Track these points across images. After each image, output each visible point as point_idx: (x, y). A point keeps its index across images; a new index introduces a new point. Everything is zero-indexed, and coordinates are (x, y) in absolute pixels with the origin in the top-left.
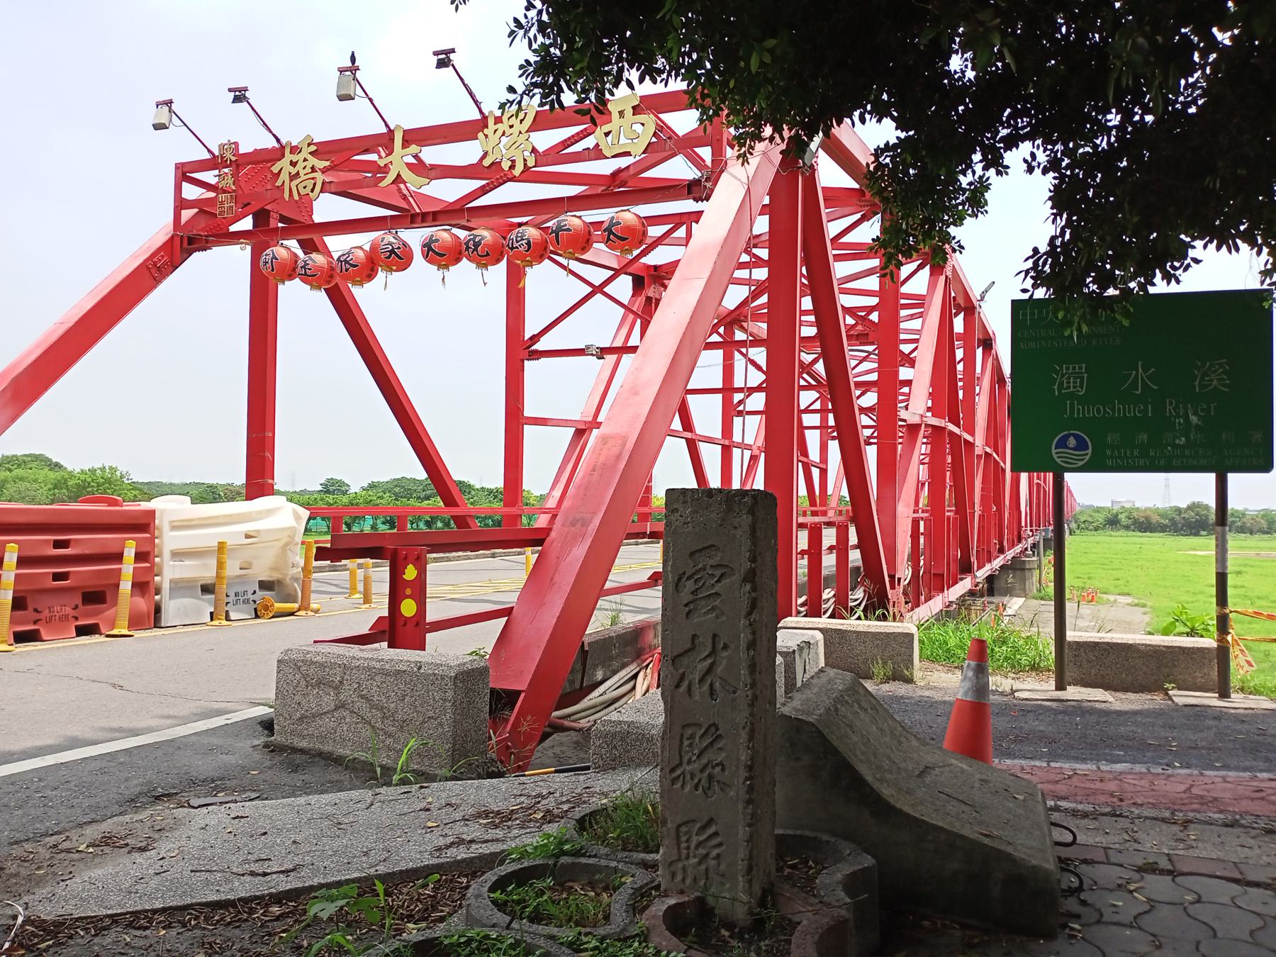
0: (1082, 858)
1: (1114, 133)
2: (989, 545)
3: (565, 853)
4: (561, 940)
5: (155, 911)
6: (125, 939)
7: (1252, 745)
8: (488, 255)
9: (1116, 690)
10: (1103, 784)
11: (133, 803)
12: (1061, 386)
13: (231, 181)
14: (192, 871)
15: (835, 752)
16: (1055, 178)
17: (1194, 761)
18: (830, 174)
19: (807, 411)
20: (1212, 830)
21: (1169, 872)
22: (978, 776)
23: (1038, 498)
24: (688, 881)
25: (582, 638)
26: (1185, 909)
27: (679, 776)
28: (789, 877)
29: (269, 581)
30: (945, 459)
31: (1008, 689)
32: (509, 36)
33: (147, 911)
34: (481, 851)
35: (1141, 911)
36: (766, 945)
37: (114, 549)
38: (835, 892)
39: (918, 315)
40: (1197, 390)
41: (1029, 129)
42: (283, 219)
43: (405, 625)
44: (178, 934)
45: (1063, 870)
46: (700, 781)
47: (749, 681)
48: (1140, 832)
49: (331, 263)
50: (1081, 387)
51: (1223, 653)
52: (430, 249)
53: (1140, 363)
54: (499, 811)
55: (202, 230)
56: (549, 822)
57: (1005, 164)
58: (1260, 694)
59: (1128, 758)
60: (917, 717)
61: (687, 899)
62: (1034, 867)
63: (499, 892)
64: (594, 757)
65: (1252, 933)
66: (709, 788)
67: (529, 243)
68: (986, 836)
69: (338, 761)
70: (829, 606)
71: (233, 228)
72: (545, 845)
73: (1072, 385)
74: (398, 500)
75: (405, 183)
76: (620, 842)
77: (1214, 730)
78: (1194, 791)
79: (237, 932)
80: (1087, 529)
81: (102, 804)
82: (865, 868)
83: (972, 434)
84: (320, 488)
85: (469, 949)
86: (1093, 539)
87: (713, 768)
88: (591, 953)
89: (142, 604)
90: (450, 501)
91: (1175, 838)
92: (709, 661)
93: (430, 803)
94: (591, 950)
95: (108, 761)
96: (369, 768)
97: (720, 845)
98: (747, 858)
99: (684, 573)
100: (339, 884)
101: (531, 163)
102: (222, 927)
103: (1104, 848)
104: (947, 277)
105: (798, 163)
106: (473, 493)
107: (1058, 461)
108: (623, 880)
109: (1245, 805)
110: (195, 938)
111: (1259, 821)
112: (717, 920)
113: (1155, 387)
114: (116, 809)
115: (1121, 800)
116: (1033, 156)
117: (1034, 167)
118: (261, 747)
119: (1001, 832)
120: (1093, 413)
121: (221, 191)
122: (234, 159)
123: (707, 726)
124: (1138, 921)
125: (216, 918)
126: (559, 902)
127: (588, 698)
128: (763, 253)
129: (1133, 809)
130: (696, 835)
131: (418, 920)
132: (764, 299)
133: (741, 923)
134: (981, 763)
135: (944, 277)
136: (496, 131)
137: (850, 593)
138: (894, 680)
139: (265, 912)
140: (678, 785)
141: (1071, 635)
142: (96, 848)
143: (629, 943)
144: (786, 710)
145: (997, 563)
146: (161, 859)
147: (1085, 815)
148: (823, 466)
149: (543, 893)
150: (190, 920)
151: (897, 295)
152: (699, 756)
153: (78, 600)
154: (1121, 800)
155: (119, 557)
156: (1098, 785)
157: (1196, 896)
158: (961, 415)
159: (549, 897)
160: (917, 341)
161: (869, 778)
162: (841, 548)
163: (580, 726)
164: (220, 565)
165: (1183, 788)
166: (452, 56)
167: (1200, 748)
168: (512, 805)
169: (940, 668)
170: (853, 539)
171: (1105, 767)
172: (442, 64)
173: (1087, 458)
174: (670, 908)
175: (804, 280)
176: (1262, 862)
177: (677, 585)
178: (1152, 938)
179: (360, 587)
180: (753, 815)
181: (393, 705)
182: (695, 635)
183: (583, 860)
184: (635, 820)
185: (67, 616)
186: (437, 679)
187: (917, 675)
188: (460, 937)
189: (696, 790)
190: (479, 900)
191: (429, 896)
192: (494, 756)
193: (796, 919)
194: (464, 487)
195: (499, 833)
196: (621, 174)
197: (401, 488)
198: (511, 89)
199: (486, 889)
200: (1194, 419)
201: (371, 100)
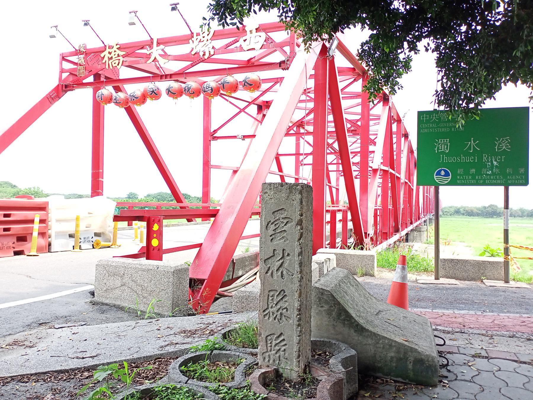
0: (448, 351)
1: (463, 34)
2: (406, 221)
3: (216, 349)
4: (210, 389)
5: (32, 375)
6: (16, 387)
7: (520, 303)
8: (194, 93)
9: (460, 280)
10: (456, 319)
11: (29, 326)
12: (438, 149)
13: (83, 61)
14: (51, 356)
15: (339, 304)
16: (438, 54)
17: (495, 309)
18: (341, 61)
19: (331, 164)
20: (504, 339)
21: (486, 357)
22: (402, 315)
23: (427, 202)
24: (271, 361)
25: (232, 257)
26: (494, 374)
27: (267, 314)
28: (317, 360)
29: (99, 233)
30: (388, 185)
31: (415, 279)
32: (207, 8)
33: (28, 374)
34: (180, 348)
35: (475, 375)
36: (306, 391)
37: (30, 218)
38: (338, 366)
39: (377, 123)
40: (497, 150)
41: (427, 33)
42: (106, 78)
43: (153, 250)
44: (41, 385)
45: (440, 356)
46: (276, 316)
47: (299, 270)
48: (473, 340)
49: (127, 97)
50: (447, 149)
51: (506, 264)
52: (169, 91)
53: (472, 139)
54: (190, 330)
55: (71, 82)
56: (212, 335)
57: (418, 49)
58: (522, 281)
59: (466, 308)
60: (376, 291)
61: (270, 370)
62: (427, 355)
63: (184, 366)
64: (234, 307)
65: (524, 384)
66: (281, 319)
67: (212, 89)
68: (406, 341)
69: (121, 308)
70: (339, 245)
71: (84, 81)
72: (207, 345)
73: (443, 148)
74: (159, 201)
75: (158, 62)
76: (242, 344)
77: (503, 296)
78: (495, 322)
79: (68, 383)
80: (447, 215)
81: (15, 327)
82: (351, 355)
83: (400, 174)
84: (127, 196)
85: (167, 393)
86: (449, 219)
87: (283, 310)
88: (224, 395)
89: (43, 242)
90: (179, 200)
91: (488, 342)
92: (281, 261)
93: (160, 327)
94: (224, 393)
95: (20, 308)
96: (136, 312)
97: (286, 345)
98: (298, 351)
99: (270, 221)
100: (108, 364)
101: (212, 53)
102: (62, 382)
103: (457, 347)
104: (390, 107)
105: (327, 54)
106: (191, 198)
107: (437, 181)
108: (242, 361)
109: (518, 328)
110: (49, 386)
111: (524, 335)
112: (284, 379)
113: (479, 149)
114: (22, 329)
115: (464, 326)
116: (428, 44)
117: (428, 49)
118: (89, 303)
119: (413, 339)
120: (452, 160)
121: (79, 65)
122: (84, 51)
123: (280, 291)
124: (473, 379)
125: (59, 378)
126: (211, 370)
127: (235, 283)
128: (312, 95)
129: (469, 330)
130: (275, 340)
131: (150, 379)
132: (312, 116)
133: (295, 381)
134: (404, 309)
135: (388, 107)
137: (348, 240)
138: (366, 275)
139: (82, 375)
140: (267, 318)
141: (442, 256)
142: (10, 346)
143: (242, 390)
144: (317, 285)
145: (410, 228)
146: (38, 351)
147: (449, 333)
148: (337, 187)
149: (204, 367)
150: (47, 378)
151: (369, 115)
152: (276, 304)
153: (15, 240)
154: (464, 326)
155: (32, 221)
156: (454, 320)
157: (499, 368)
158: (395, 166)
159: (207, 369)
160: (377, 134)
161: (354, 315)
162: (344, 221)
163: (231, 295)
164: (77, 226)
165: (491, 321)
166: (178, 6)
167: (497, 304)
168: (196, 327)
169: (385, 270)
170: (349, 217)
171: (456, 312)
172: (173, 9)
173: (449, 180)
174: (263, 373)
175: (329, 107)
176: (526, 353)
177: (267, 227)
178: (480, 387)
179: (139, 236)
180: (301, 331)
181: (146, 284)
182: (275, 249)
183: (224, 352)
184: (249, 334)
185: (10, 247)
186: (165, 273)
187: (376, 273)
188: (163, 387)
189: (275, 320)
190: (174, 370)
191: (156, 368)
192: (191, 307)
193: (320, 378)
194: (187, 196)
195: (189, 340)
196: (251, 60)
197: (160, 197)
198: (204, 19)
199: (178, 365)
200: (495, 163)
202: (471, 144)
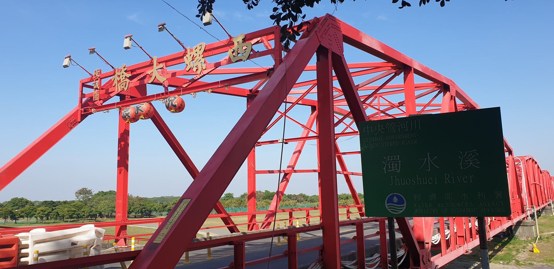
40: (462, 168)
53: (428, 153)
107: (389, 210)
113: (438, 167)
136: (190, 55)
173: (404, 208)
201: (141, 47)
202: (427, 160)
